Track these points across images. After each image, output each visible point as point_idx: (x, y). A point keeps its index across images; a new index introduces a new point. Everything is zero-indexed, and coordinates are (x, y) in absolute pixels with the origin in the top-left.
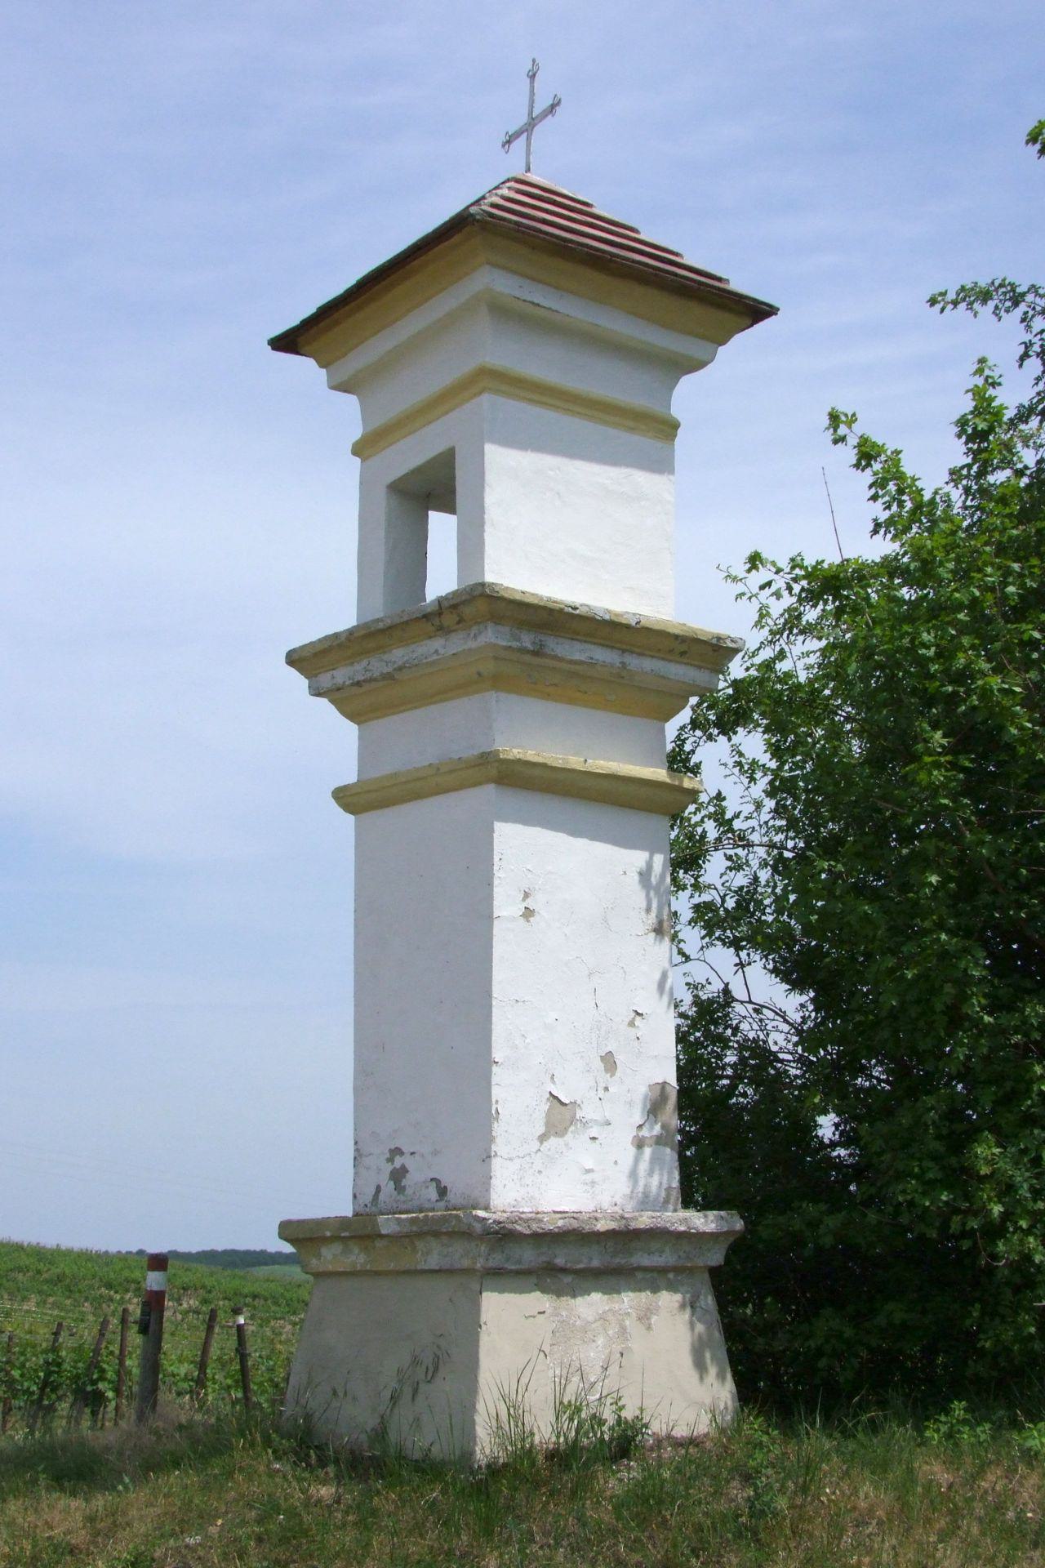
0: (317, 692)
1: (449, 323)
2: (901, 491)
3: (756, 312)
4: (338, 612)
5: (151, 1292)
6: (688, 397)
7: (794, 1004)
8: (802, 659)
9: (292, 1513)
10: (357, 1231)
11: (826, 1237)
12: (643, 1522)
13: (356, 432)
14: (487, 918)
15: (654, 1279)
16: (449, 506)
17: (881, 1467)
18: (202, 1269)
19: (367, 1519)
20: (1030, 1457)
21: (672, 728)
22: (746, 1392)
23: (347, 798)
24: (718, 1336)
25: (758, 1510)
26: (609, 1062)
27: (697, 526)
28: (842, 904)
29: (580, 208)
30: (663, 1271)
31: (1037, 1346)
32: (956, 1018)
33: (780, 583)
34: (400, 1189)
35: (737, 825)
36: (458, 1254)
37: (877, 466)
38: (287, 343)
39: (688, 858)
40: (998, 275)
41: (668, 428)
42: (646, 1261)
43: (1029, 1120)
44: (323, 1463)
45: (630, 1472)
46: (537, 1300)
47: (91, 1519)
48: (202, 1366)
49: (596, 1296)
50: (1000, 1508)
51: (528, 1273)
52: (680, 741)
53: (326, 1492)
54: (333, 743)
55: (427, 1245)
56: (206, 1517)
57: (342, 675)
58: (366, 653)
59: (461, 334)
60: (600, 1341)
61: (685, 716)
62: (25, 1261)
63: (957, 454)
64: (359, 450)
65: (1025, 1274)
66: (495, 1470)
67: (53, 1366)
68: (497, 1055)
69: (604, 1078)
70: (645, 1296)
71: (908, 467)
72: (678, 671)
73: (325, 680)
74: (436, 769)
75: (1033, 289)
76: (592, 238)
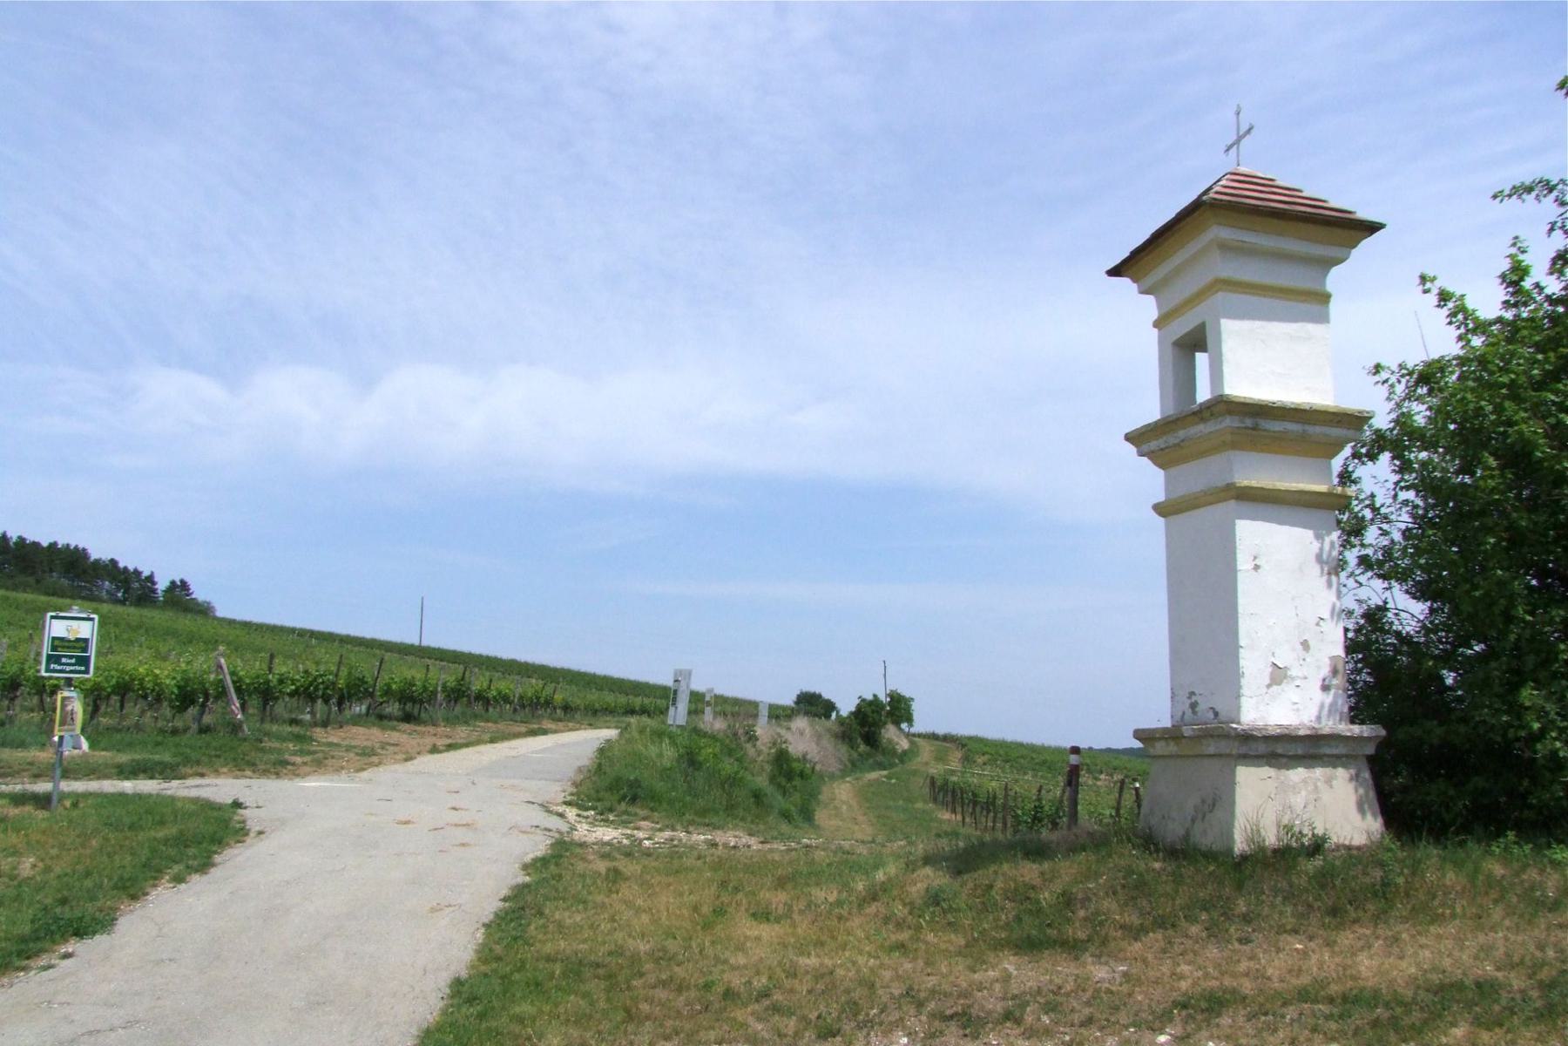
0: (1141, 454)
1: (1194, 259)
2: (1466, 318)
3: (1372, 228)
4: (1150, 410)
5: (1074, 767)
6: (1336, 279)
7: (1419, 608)
8: (1420, 414)
9: (1141, 875)
10: (1172, 735)
11: (1431, 739)
12: (1323, 886)
13: (1154, 315)
14: (1231, 570)
15: (1334, 761)
16: (1204, 350)
17: (1458, 865)
18: (1125, 758)
19: (1178, 879)
20: (1556, 864)
21: (1337, 463)
22: (1388, 823)
23: (1160, 509)
24: (1372, 794)
25: (1385, 884)
26: (1305, 645)
27: (1350, 350)
28: (1444, 553)
29: (1268, 184)
30: (1338, 757)
31: (1565, 803)
32: (1509, 618)
33: (1393, 379)
34: (1194, 712)
35: (1383, 511)
36: (1223, 747)
37: (1450, 305)
38: (1115, 272)
39: (1355, 530)
40: (1538, 177)
41: (1325, 298)
42: (1328, 751)
43: (1555, 676)
44: (1157, 851)
45: (1318, 862)
46: (1267, 771)
47: (1042, 873)
48: (1118, 810)
49: (1300, 770)
50: (1532, 889)
51: (1258, 757)
52: (1345, 466)
53: (1157, 865)
54: (1151, 481)
55: (1208, 742)
56: (1097, 875)
57: (1153, 445)
58: (1164, 433)
59: (1205, 257)
60: (1304, 793)
61: (1347, 451)
62: (1025, 752)
63: (1500, 293)
64: (1157, 324)
65: (1554, 760)
66: (1244, 858)
67: (1038, 808)
68: (1242, 643)
69: (1302, 653)
70: (1329, 770)
71: (1470, 304)
72: (1336, 432)
73: (1145, 448)
74: (1205, 493)
75: (1562, 181)
76: (1275, 201)
